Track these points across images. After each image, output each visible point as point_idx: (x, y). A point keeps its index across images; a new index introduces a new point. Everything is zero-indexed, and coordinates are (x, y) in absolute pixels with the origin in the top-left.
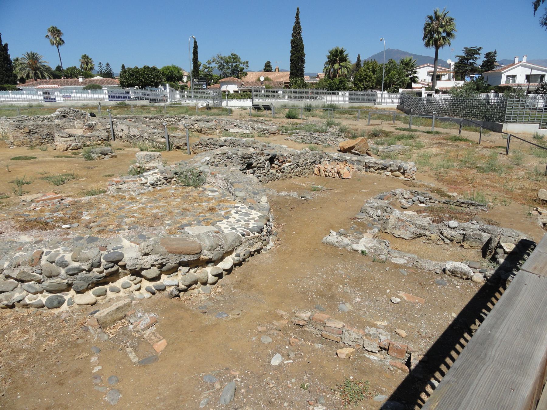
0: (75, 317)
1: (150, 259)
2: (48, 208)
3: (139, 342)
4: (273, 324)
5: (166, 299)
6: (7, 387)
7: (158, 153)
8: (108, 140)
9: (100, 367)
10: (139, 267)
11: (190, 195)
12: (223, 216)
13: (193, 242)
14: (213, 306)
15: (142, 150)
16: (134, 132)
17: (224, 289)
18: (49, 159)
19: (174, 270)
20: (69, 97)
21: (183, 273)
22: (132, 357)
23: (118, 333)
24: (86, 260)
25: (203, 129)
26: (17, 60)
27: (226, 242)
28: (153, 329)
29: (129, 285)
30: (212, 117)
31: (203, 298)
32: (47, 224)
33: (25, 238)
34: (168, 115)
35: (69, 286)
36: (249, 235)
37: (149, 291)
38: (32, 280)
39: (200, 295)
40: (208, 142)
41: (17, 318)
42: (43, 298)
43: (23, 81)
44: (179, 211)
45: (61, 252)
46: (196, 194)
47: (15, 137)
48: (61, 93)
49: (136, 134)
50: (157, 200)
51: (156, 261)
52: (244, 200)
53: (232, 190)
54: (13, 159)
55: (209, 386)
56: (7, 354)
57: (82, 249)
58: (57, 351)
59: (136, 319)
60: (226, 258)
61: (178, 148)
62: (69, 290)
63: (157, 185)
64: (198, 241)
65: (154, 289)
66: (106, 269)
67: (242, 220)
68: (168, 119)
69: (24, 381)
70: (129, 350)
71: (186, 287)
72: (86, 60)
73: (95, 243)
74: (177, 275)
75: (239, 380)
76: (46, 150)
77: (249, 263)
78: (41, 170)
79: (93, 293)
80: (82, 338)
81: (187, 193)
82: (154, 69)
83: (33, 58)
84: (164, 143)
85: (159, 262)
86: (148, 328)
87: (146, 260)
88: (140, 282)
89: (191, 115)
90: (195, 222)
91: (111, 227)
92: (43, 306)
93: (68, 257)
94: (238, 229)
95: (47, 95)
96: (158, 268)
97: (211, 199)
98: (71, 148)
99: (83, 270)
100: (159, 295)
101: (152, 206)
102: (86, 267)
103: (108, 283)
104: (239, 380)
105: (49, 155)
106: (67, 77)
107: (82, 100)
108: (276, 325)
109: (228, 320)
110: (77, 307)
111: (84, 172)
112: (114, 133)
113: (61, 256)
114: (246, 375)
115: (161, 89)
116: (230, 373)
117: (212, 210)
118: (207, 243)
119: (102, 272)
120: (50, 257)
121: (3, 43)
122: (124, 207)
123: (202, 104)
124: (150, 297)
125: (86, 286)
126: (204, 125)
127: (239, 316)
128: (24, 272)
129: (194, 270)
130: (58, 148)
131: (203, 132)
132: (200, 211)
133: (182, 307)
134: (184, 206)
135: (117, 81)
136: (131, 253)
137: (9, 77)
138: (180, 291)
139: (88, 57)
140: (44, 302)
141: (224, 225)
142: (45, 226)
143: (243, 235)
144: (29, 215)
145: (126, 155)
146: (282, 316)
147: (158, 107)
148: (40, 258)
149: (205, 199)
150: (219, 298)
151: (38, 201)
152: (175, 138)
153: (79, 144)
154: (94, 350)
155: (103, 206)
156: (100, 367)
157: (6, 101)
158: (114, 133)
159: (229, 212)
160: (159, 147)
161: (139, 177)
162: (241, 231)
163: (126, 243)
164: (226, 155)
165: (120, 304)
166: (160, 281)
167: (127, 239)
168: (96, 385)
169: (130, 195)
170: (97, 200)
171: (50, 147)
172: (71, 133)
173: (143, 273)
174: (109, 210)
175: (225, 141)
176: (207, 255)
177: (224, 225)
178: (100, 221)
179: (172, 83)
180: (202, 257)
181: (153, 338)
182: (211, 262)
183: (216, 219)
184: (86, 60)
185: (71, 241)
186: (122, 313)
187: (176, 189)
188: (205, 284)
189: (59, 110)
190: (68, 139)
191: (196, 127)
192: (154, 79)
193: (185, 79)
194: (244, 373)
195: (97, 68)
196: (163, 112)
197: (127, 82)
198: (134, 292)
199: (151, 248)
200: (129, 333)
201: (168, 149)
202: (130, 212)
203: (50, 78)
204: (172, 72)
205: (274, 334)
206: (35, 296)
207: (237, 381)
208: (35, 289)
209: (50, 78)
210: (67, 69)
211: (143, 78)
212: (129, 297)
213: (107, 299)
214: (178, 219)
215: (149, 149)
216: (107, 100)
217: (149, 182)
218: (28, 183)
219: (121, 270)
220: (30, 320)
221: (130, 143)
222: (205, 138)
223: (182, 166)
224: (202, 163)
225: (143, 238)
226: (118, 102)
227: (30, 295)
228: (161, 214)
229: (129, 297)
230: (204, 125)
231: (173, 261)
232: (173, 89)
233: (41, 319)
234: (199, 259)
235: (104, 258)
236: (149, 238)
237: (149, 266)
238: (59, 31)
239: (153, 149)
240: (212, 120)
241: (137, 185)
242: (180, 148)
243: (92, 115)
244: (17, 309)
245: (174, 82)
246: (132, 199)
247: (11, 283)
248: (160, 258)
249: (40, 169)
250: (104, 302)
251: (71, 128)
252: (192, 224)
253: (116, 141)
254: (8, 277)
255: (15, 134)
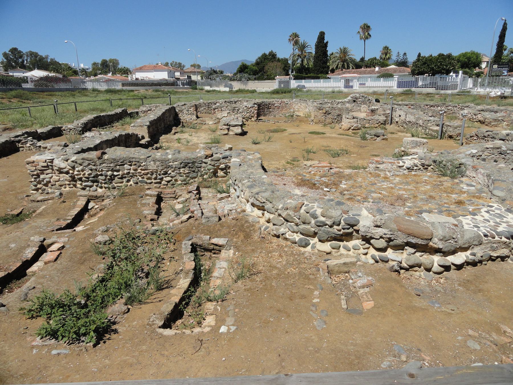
0: (314, 259)
1: (380, 231)
2: (319, 173)
3: (352, 295)
4: (490, 336)
5: (386, 271)
6: (261, 286)
7: (425, 140)
8: (385, 124)
9: (318, 300)
10: (369, 235)
11: (442, 185)
12: (470, 212)
13: (425, 228)
14: (429, 293)
15: (413, 136)
16: (411, 118)
17: (447, 282)
18: (334, 135)
19: (400, 248)
20: (364, 84)
21: (408, 253)
22: (343, 304)
23: (340, 282)
24: (331, 217)
25: (486, 120)
26: (332, 54)
27: (462, 237)
28: (367, 290)
29: (358, 248)
30: (502, 108)
31: (422, 283)
32: (315, 184)
33: (298, 192)
34: (450, 103)
35: (315, 234)
36: (494, 238)
37: (373, 259)
38: (293, 222)
39: (420, 279)
40: (486, 134)
41: (278, 245)
42: (297, 237)
43: (333, 71)
44: (424, 197)
45: (315, 207)
46: (450, 185)
47: (316, 116)
48: (358, 81)
49: (411, 121)
50: (408, 183)
51: (385, 234)
52: (503, 200)
53: (491, 188)
54: (309, 133)
55: (396, 354)
56: (267, 266)
57: (330, 208)
58: (295, 277)
59: (356, 277)
60: (459, 253)
61: (451, 137)
62: (314, 237)
63: (413, 170)
64: (431, 228)
65: (378, 258)
66: (343, 229)
67: (491, 221)
68: (449, 108)
69: (271, 287)
70: (343, 297)
71: (408, 267)
72: (386, 51)
73: (341, 206)
74: (402, 253)
75: (427, 364)
76: (334, 128)
77: (486, 266)
78: (325, 144)
79: (330, 245)
80: (313, 275)
81: (440, 182)
82: (449, 56)
83: (344, 52)
84: (437, 131)
85: (388, 236)
86: (363, 287)
87: (376, 231)
88: (368, 248)
89: (478, 104)
90: (436, 211)
91: (359, 198)
92: (296, 243)
93: (319, 211)
94: (482, 228)
95: (348, 84)
96: (386, 241)
97: (465, 192)
98: (352, 128)
99: (326, 225)
100: (381, 265)
101: (401, 188)
102: (329, 223)
103: (343, 241)
104: (427, 364)
105: (335, 133)
106: (367, 67)
107: (374, 87)
108: (493, 338)
109: (439, 310)
110: (317, 251)
111: (356, 150)
112: (392, 118)
113: (314, 209)
114: (437, 364)
115: (452, 76)
116: (420, 354)
117: (460, 203)
118: (440, 232)
119: (340, 231)
120: (307, 209)
121: (325, 41)
122: (376, 184)
123: (496, 92)
124: (374, 264)
125: (326, 238)
126: (493, 115)
127: (453, 312)
128: (289, 215)
129: (420, 254)
130: (343, 127)
131: (486, 123)
132: (446, 201)
133: (398, 282)
134: (431, 194)
135: (409, 70)
136: (366, 221)
137: (323, 68)
138: (402, 268)
139: (388, 48)
140: (297, 240)
141: (467, 222)
142: (313, 186)
143: (486, 236)
144: (305, 176)
145: (396, 139)
146: (505, 332)
147: (444, 94)
148: (301, 208)
149: (457, 191)
150: (439, 289)
151: (315, 167)
152: (449, 127)
153: (360, 126)
154: (318, 286)
155: (360, 180)
156: (318, 300)
157: (317, 87)
158: (392, 118)
159: (480, 209)
160: (431, 135)
161: (398, 160)
162: (484, 231)
163: (365, 212)
164: (499, 150)
165: (348, 260)
166: (386, 253)
167: (366, 209)
168: (312, 310)
169: (385, 174)
170: (356, 174)
171: (337, 126)
172: (355, 116)
173: (372, 241)
174: (363, 183)
175: (508, 135)
176: (436, 243)
177: (467, 222)
178: (352, 191)
179: (467, 70)
180: (431, 244)
181: (365, 297)
182: (440, 252)
183: (460, 213)
184: (386, 51)
185: (325, 200)
186: (347, 269)
187: (430, 177)
188: (429, 270)
189: (351, 95)
190: (352, 120)
191: (480, 117)
192: (446, 66)
193: (484, 65)
194: (435, 362)
195: (394, 57)
196: (448, 100)
197: (418, 70)
198: (361, 255)
199: (383, 222)
200: (348, 286)
201: (439, 137)
202: (379, 189)
203: (353, 68)
204: (469, 59)
205: (485, 344)
206: (293, 234)
207: (425, 364)
208: (294, 229)
209: (353, 68)
210: (369, 60)
211: (435, 66)
212: (356, 257)
213: (339, 253)
214: (420, 203)
215: (420, 136)
216: (395, 88)
217: (406, 165)
218: (314, 153)
219: (354, 233)
220: (286, 249)
221: (405, 128)
222: (484, 129)
223: (443, 155)
224: (466, 155)
225: (380, 211)
226: (405, 89)
227: (290, 232)
228: (406, 196)
229: (356, 257)
230: (488, 116)
231: (401, 239)
232: (466, 76)
233: (292, 251)
234: (427, 245)
235: (343, 220)
236: (385, 214)
237: (378, 237)
238: (369, 27)
239: (425, 136)
240: (502, 111)
241: (394, 166)
242: (452, 138)
243: (377, 101)
244: (280, 239)
245: (469, 68)
246: (386, 178)
247: (281, 220)
248: (390, 233)
249: (324, 143)
250: (336, 255)
251: (357, 111)
252: (432, 212)
253: (392, 125)
254: (280, 215)
255: (316, 113)
